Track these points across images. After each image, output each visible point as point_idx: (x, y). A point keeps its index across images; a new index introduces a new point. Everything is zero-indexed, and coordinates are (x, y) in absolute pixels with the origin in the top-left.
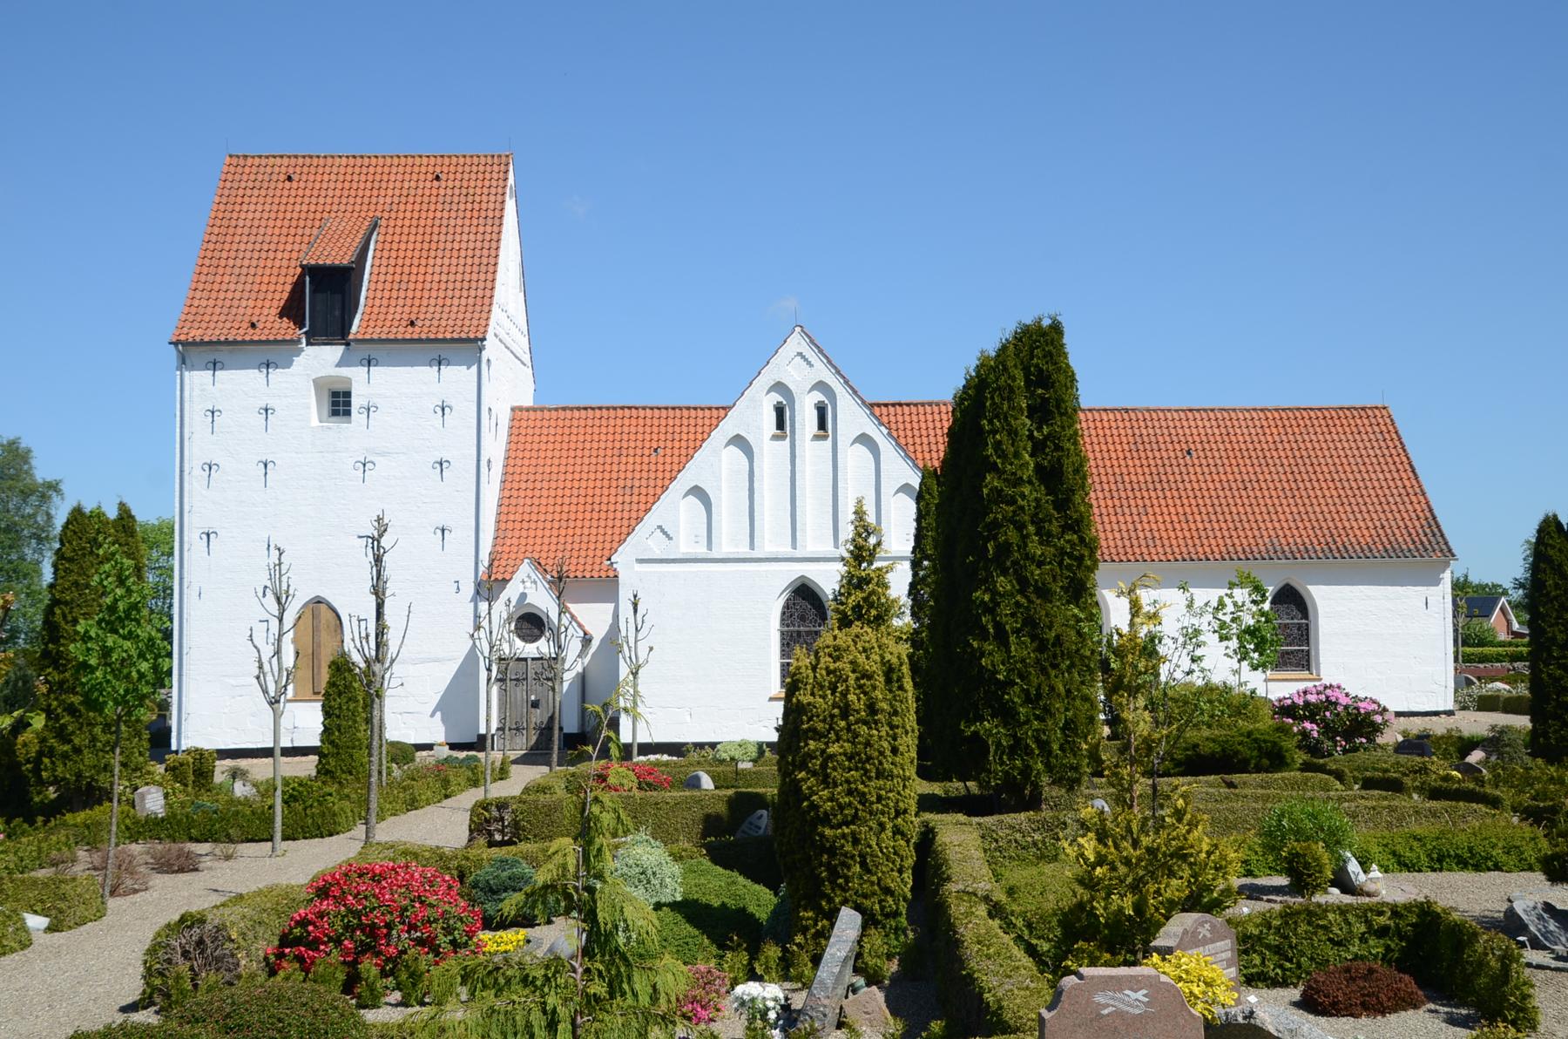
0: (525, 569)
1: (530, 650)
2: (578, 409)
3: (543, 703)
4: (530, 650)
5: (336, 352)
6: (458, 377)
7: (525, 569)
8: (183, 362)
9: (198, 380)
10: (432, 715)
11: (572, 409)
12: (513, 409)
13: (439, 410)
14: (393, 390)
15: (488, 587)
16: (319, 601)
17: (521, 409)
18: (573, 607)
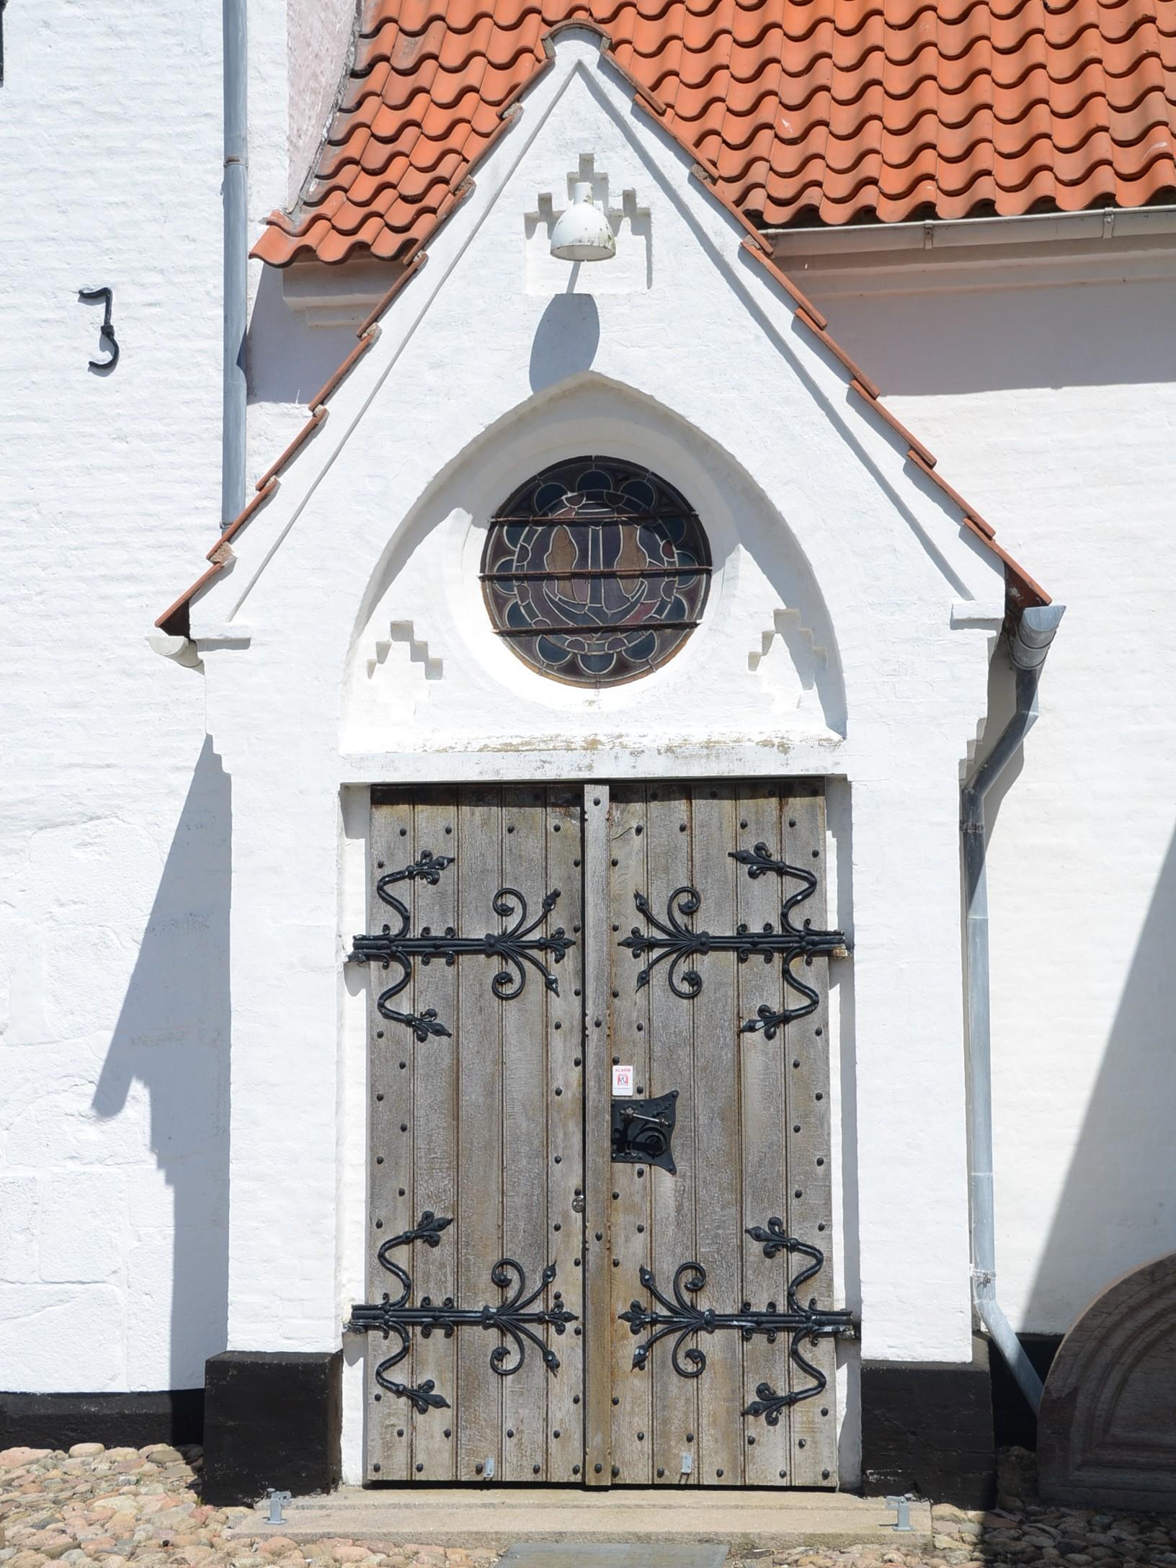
0: (570, 118)
3: (698, 1127)
7: (570, 118)
10: (108, 1101)
15: (324, 286)
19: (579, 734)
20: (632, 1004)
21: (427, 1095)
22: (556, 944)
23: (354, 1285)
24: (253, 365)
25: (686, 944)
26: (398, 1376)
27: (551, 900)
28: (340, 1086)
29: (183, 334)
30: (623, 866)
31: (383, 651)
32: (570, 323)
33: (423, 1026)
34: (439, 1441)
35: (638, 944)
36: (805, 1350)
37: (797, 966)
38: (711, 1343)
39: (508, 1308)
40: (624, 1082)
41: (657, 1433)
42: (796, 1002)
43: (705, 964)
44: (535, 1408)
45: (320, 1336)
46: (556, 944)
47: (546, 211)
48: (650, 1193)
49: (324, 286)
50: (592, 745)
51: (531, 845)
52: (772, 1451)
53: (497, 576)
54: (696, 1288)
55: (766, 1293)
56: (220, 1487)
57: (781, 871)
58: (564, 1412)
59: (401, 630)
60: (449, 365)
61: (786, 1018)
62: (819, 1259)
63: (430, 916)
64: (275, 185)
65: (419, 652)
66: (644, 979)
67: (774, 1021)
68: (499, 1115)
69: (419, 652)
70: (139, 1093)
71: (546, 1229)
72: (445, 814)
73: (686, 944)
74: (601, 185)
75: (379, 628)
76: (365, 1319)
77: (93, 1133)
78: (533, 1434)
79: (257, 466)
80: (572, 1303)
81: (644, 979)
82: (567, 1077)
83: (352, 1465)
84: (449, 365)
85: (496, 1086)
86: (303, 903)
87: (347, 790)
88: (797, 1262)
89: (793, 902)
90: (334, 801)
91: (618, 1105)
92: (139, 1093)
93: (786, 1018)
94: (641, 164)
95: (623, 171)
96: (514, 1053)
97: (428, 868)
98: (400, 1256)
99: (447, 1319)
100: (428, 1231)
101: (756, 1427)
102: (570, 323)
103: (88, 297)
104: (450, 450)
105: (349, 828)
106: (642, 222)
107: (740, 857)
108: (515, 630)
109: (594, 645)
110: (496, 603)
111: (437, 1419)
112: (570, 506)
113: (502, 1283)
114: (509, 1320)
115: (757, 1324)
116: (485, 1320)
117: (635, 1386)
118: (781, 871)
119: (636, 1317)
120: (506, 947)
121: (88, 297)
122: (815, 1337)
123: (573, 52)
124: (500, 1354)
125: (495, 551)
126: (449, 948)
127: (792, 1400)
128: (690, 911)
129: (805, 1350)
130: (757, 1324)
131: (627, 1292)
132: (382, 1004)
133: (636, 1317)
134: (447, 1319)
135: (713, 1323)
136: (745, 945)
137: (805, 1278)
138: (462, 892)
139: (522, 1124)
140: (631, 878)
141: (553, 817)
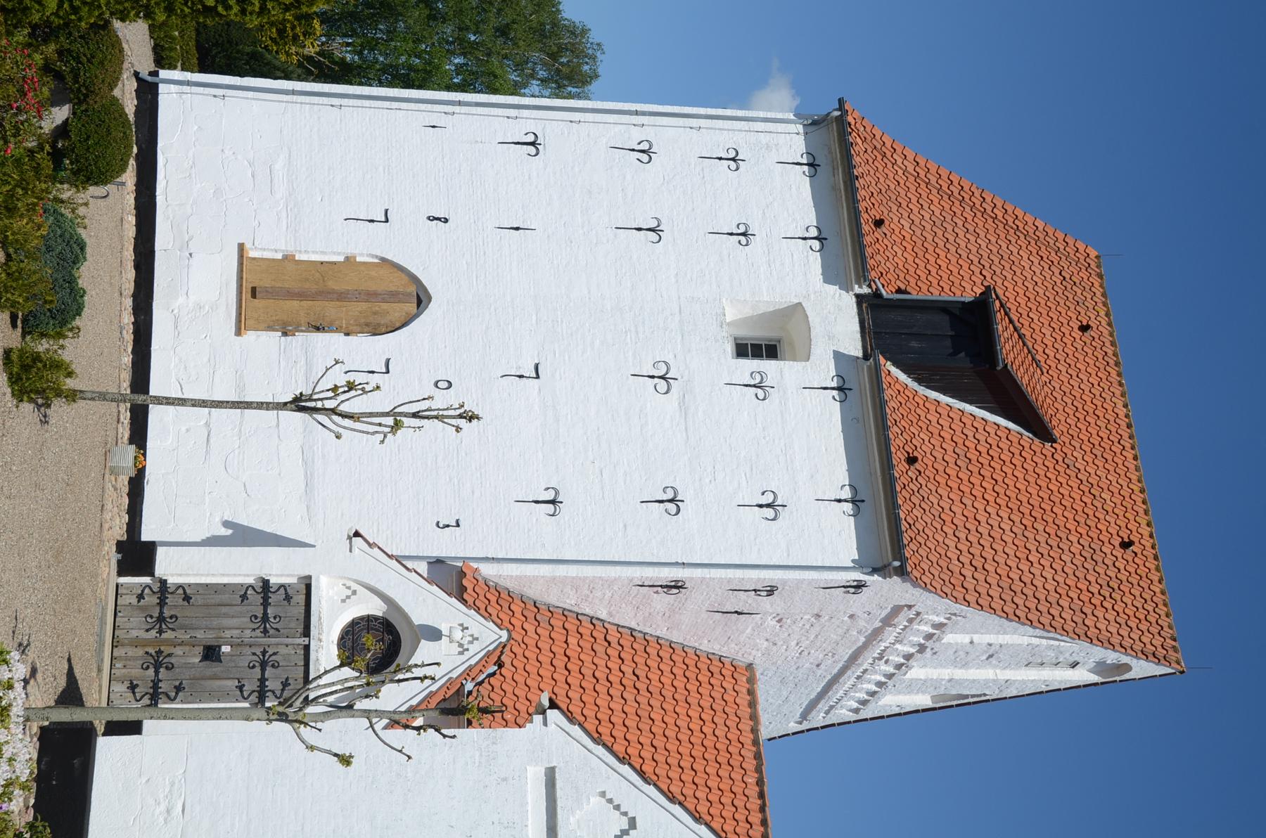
0: (489, 635)
1: (326, 652)
2: (760, 783)
3: (215, 668)
4: (326, 652)
5: (853, 346)
6: (837, 538)
7: (489, 635)
8: (814, 124)
9: (793, 142)
10: (227, 524)
11: (759, 769)
12: (750, 667)
13: (768, 499)
14: (800, 434)
15: (453, 578)
16: (422, 300)
17: (751, 680)
18: (412, 662)
19: (324, 637)
20: (248, 651)
21: (225, 598)
22: (265, 631)
23: (172, 580)
24: (437, 563)
25: (263, 665)
26: (147, 590)
27: (277, 630)
28: (228, 575)
29: (449, 546)
30: (285, 648)
31: (349, 588)
32: (434, 634)
33: (244, 597)
34: (128, 602)
35: (264, 653)
36: (148, 696)
37: (256, 694)
38: (151, 672)
39: (164, 619)
40: (226, 649)
41: (127, 658)
42: (246, 694)
43: (258, 670)
44: (136, 627)
45: (160, 570)
46: (265, 631)
47: (465, 629)
48: (194, 655)
49: (453, 578)
50: (320, 640)
51: (293, 625)
52: (120, 688)
53: (369, 619)
54: (167, 668)
55: (164, 686)
56: (120, 546)
57: (283, 690)
58: (134, 633)
59: (354, 592)
60: (425, 604)
61: (241, 691)
62: (172, 700)
63: (273, 599)
64: (487, 570)
65: (348, 597)
66: (254, 654)
67: (241, 688)
68: (218, 616)
69: (348, 597)
70: (230, 532)
71: (185, 628)
72: (303, 603)
73: (263, 665)
74: (471, 642)
75: (355, 586)
76: (163, 583)
77: (218, 519)
78: (128, 625)
79: (409, 564)
80: (164, 636)
81: (254, 654)
82: (228, 634)
83: (123, 580)
84: (425, 604)
85: (226, 615)
86: (280, 568)
87: (310, 577)
88: (172, 694)
89: (273, 692)
90: (307, 573)
91: (220, 647)
92: (230, 532)
93: (241, 691)
94: (476, 653)
95: (474, 648)
96: (235, 620)
97: (288, 598)
98: (180, 591)
99: (162, 603)
100: (187, 598)
101: (127, 684)
102: (434, 634)
103: (457, 521)
104: (401, 603)
105: (300, 578)
106: (461, 653)
107: (287, 679)
108: (354, 623)
109: (349, 644)
110: (362, 618)
111: (134, 601)
112: (388, 638)
113: (171, 617)
114: (161, 619)
115: (155, 685)
116: (161, 613)
117: (140, 652)
118: (283, 690)
119: (159, 652)
120: (265, 618)
121: (457, 521)
122: (151, 699)
123: (504, 635)
124: (151, 617)
125: (376, 618)
126: (266, 604)
127: (134, 693)
128: (273, 666)
129: (148, 696)
130: (155, 685)
131: (166, 650)
132: (251, 586)
133: (159, 652)
134: (162, 603)
135: (157, 673)
136: (262, 680)
137: (168, 697)
138: (279, 609)
139: (215, 622)
140: (283, 650)
141: (300, 630)
